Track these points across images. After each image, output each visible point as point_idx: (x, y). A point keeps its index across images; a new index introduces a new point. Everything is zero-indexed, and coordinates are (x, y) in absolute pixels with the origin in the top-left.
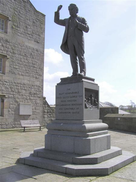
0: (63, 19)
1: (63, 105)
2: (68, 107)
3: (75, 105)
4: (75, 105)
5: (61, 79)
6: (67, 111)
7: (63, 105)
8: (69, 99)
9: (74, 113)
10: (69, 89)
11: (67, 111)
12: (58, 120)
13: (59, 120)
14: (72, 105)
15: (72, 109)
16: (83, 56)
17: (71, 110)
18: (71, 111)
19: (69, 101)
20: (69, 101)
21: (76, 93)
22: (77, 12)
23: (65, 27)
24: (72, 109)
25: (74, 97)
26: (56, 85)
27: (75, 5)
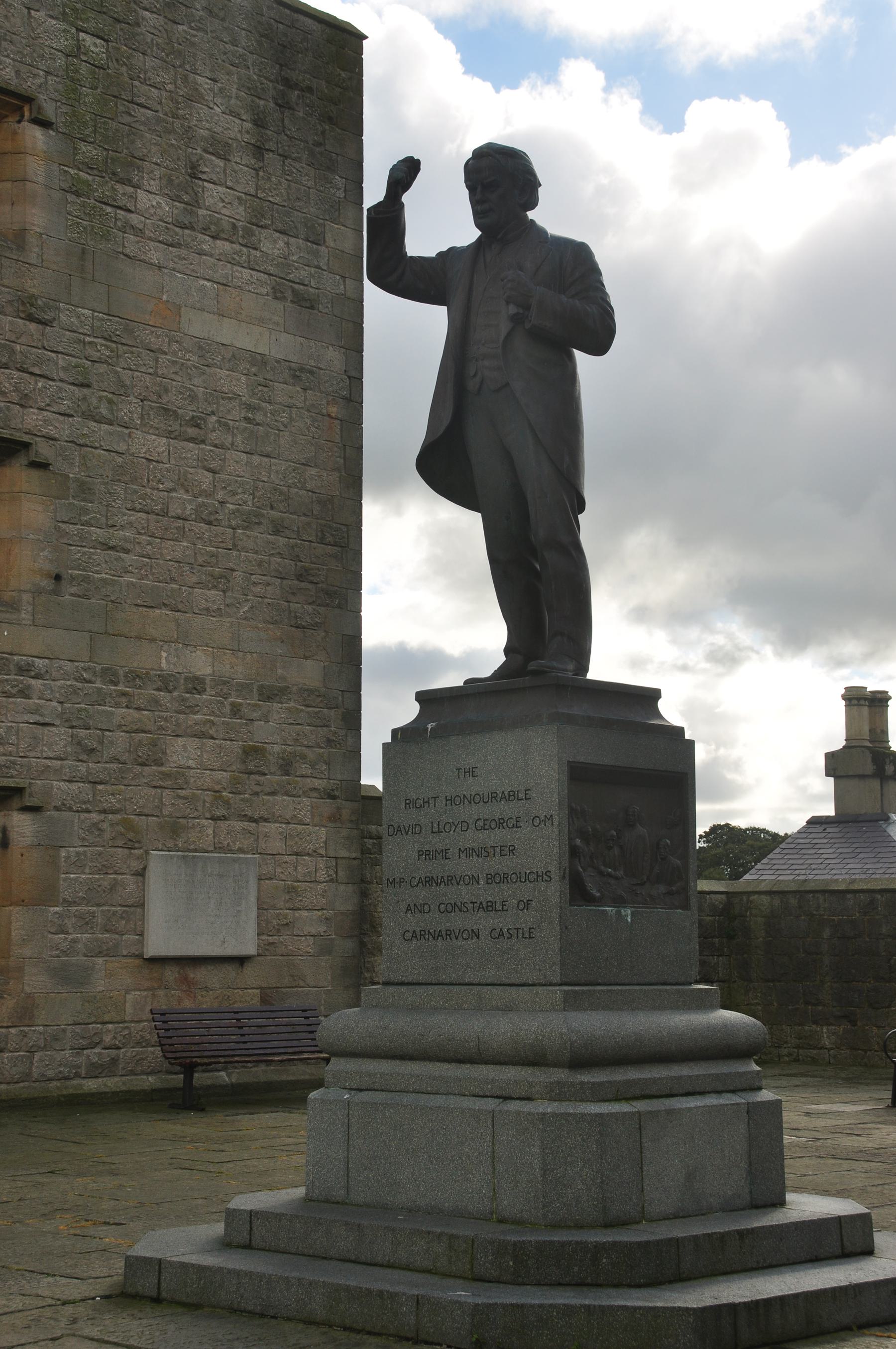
0: (433, 254)
1: (429, 881)
2: (464, 893)
3: (505, 878)
4: (505, 878)
5: (845, 688)
6: (457, 921)
7: (429, 881)
8: (472, 839)
9: (501, 934)
10: (471, 772)
11: (457, 921)
12: (402, 984)
13: (403, 989)
14: (491, 879)
15: (489, 907)
16: (659, 716)
17: (481, 913)
18: (484, 922)
19: (468, 852)
20: (468, 852)
21: (511, 796)
22: (532, 203)
23: (445, 308)
24: (489, 907)
25: (501, 823)
26: (389, 740)
27: (537, 205)
